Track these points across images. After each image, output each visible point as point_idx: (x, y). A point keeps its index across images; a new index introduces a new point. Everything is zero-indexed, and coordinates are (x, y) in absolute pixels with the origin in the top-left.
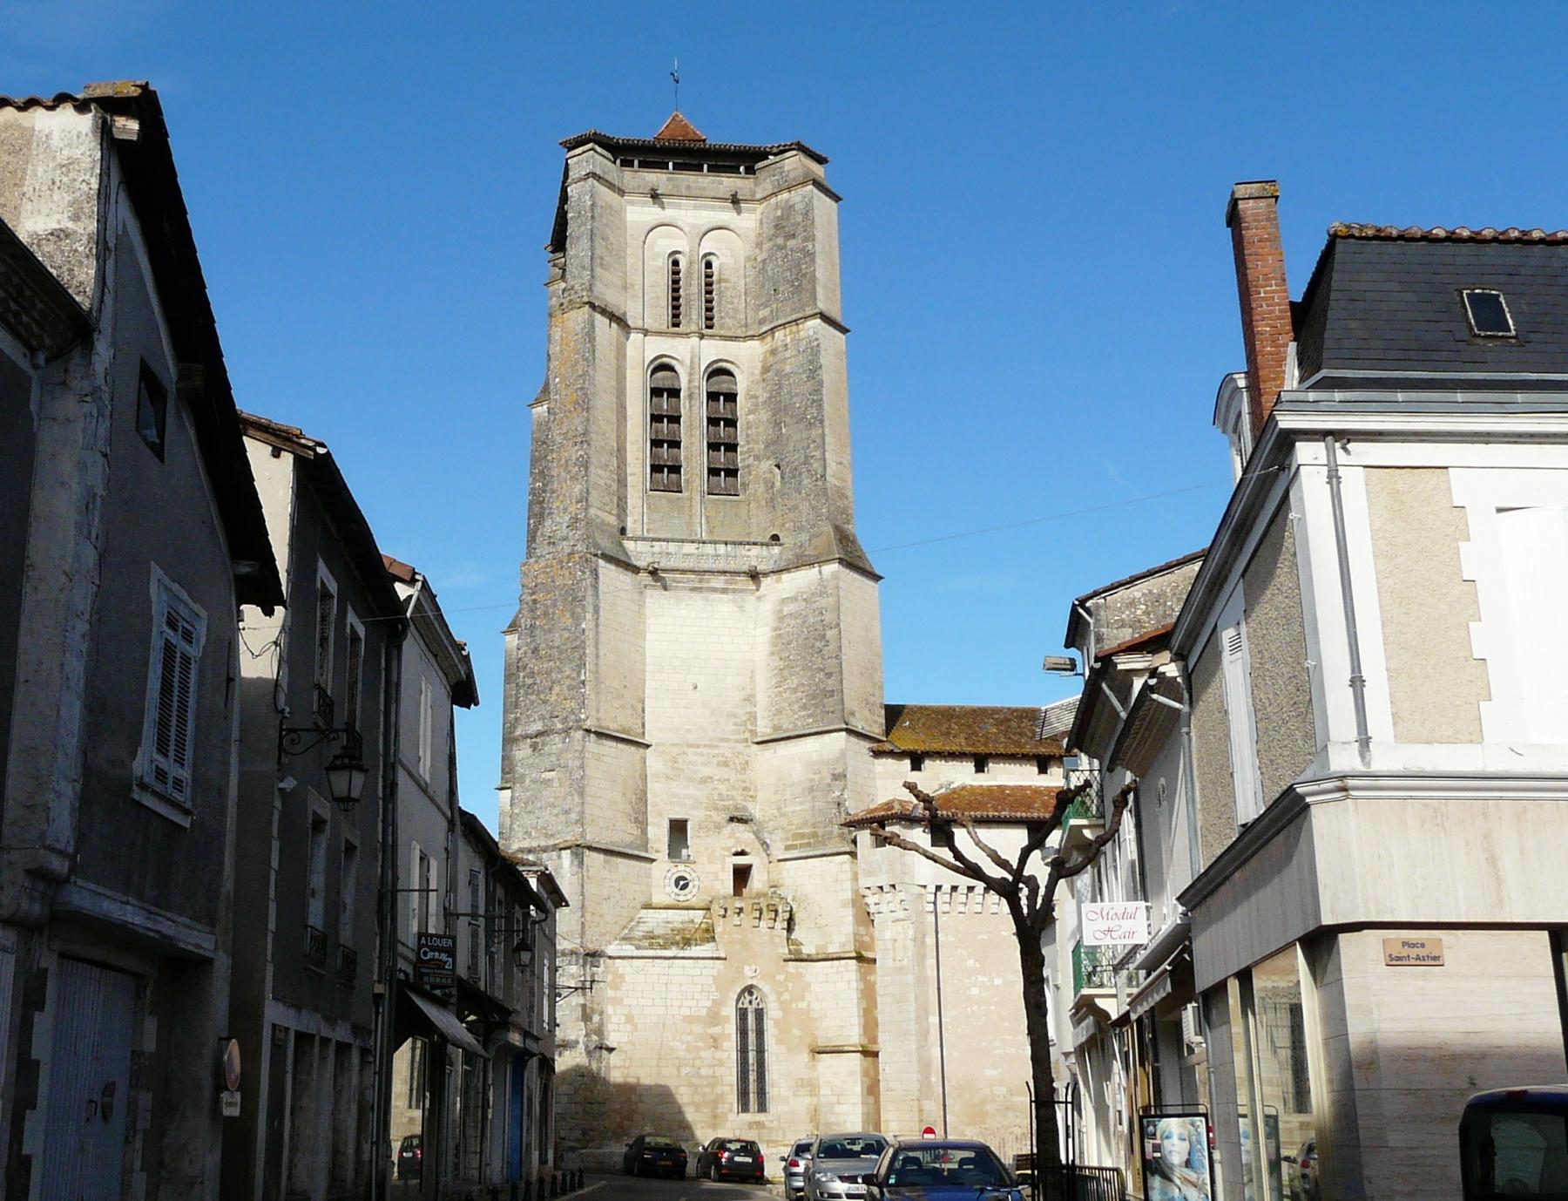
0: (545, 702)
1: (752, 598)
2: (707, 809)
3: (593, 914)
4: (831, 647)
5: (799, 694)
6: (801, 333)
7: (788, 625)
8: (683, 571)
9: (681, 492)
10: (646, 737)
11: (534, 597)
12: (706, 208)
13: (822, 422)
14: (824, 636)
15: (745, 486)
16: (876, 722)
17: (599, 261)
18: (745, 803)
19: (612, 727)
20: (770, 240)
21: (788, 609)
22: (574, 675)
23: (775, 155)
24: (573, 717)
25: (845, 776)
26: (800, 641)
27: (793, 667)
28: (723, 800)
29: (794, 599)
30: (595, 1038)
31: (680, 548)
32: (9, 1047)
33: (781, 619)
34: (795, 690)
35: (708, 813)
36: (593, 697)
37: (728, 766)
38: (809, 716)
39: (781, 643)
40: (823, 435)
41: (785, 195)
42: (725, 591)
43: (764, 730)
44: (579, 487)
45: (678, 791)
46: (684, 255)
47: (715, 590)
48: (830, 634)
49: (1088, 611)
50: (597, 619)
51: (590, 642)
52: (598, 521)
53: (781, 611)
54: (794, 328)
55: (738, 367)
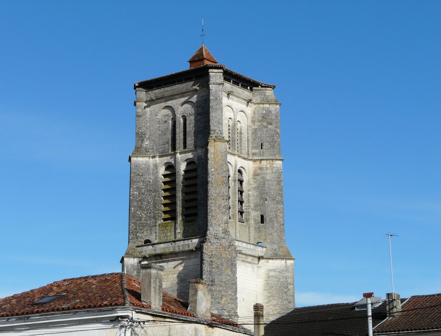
0: (219, 303)
1: (256, 266)
4: (290, 292)
6: (274, 165)
9: (244, 223)
11: (211, 259)
14: (287, 287)
20: (260, 122)
21: (272, 274)
22: (233, 294)
23: (262, 87)
24: (233, 311)
27: (274, 297)
29: (274, 270)
31: (242, 244)
33: (269, 277)
41: (267, 106)
42: (250, 263)
44: (226, 217)
46: (232, 120)
47: (248, 262)
48: (290, 287)
53: (268, 274)
54: (271, 162)
55: (245, 170)
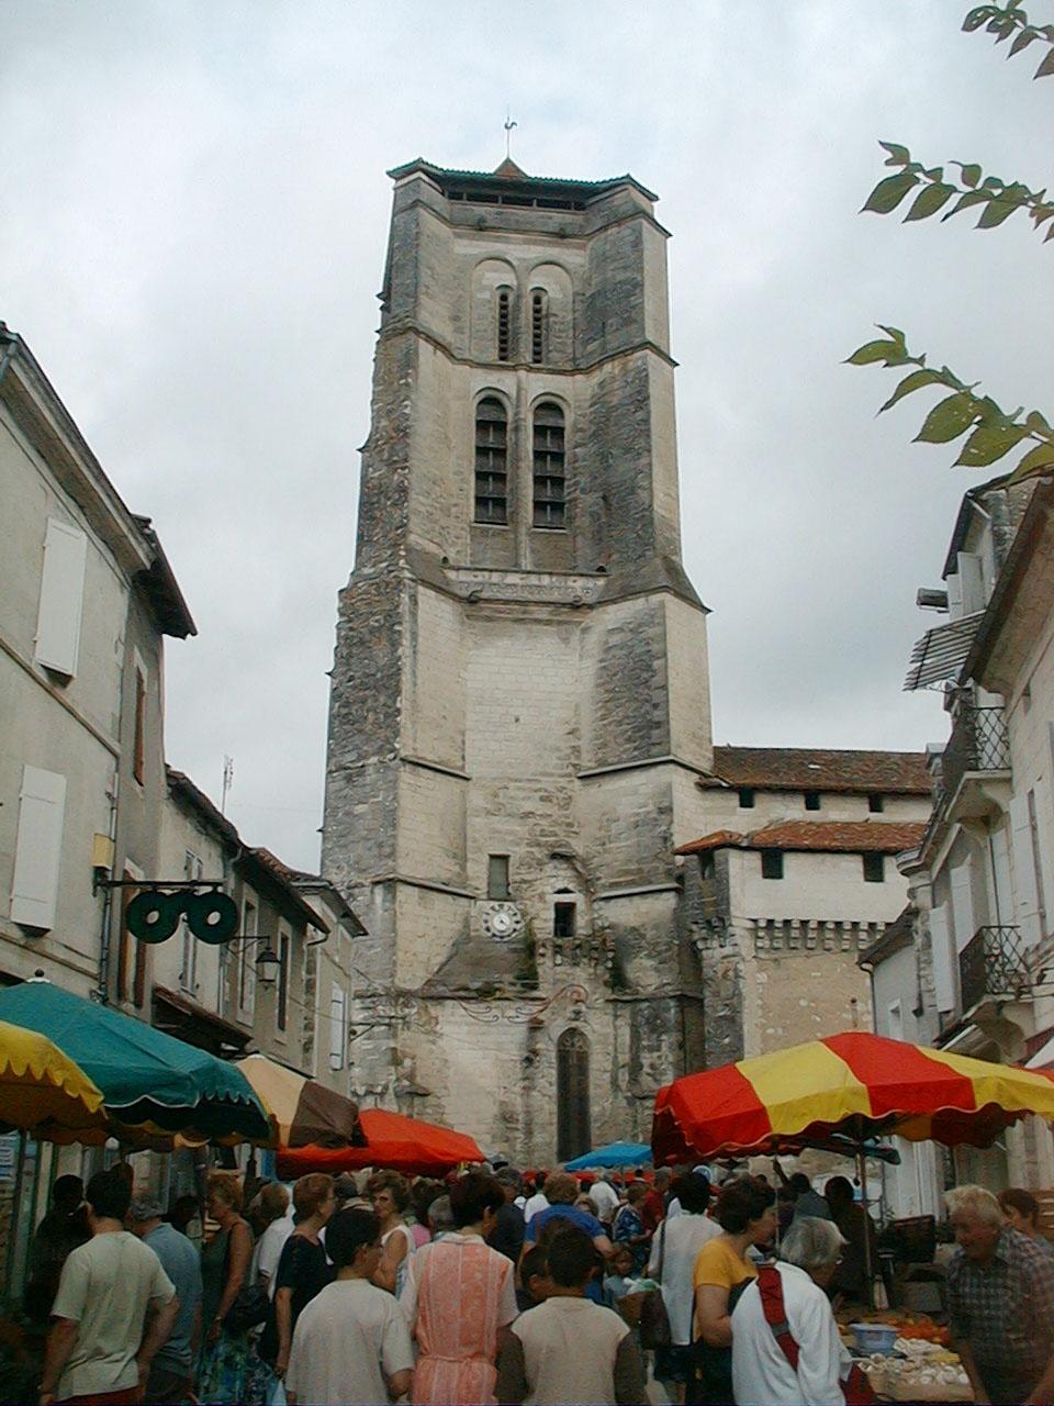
2: (528, 845)
3: (406, 952)
5: (624, 727)
7: (614, 656)
8: (507, 602)
9: (506, 524)
10: (467, 770)
12: (535, 243)
13: (649, 451)
14: (650, 666)
15: (571, 519)
16: (704, 757)
17: (424, 289)
18: (567, 839)
19: (429, 756)
21: (615, 639)
25: (671, 810)
26: (626, 672)
28: (546, 836)
30: (406, 1083)
32: (936, 1160)
34: (620, 723)
35: (529, 849)
36: (409, 726)
37: (551, 801)
38: (635, 749)
39: (606, 673)
40: (650, 464)
42: (548, 622)
43: (589, 764)
45: (499, 826)
48: (656, 664)
49: (983, 504)
50: (415, 646)
51: (407, 670)
52: (418, 548)
